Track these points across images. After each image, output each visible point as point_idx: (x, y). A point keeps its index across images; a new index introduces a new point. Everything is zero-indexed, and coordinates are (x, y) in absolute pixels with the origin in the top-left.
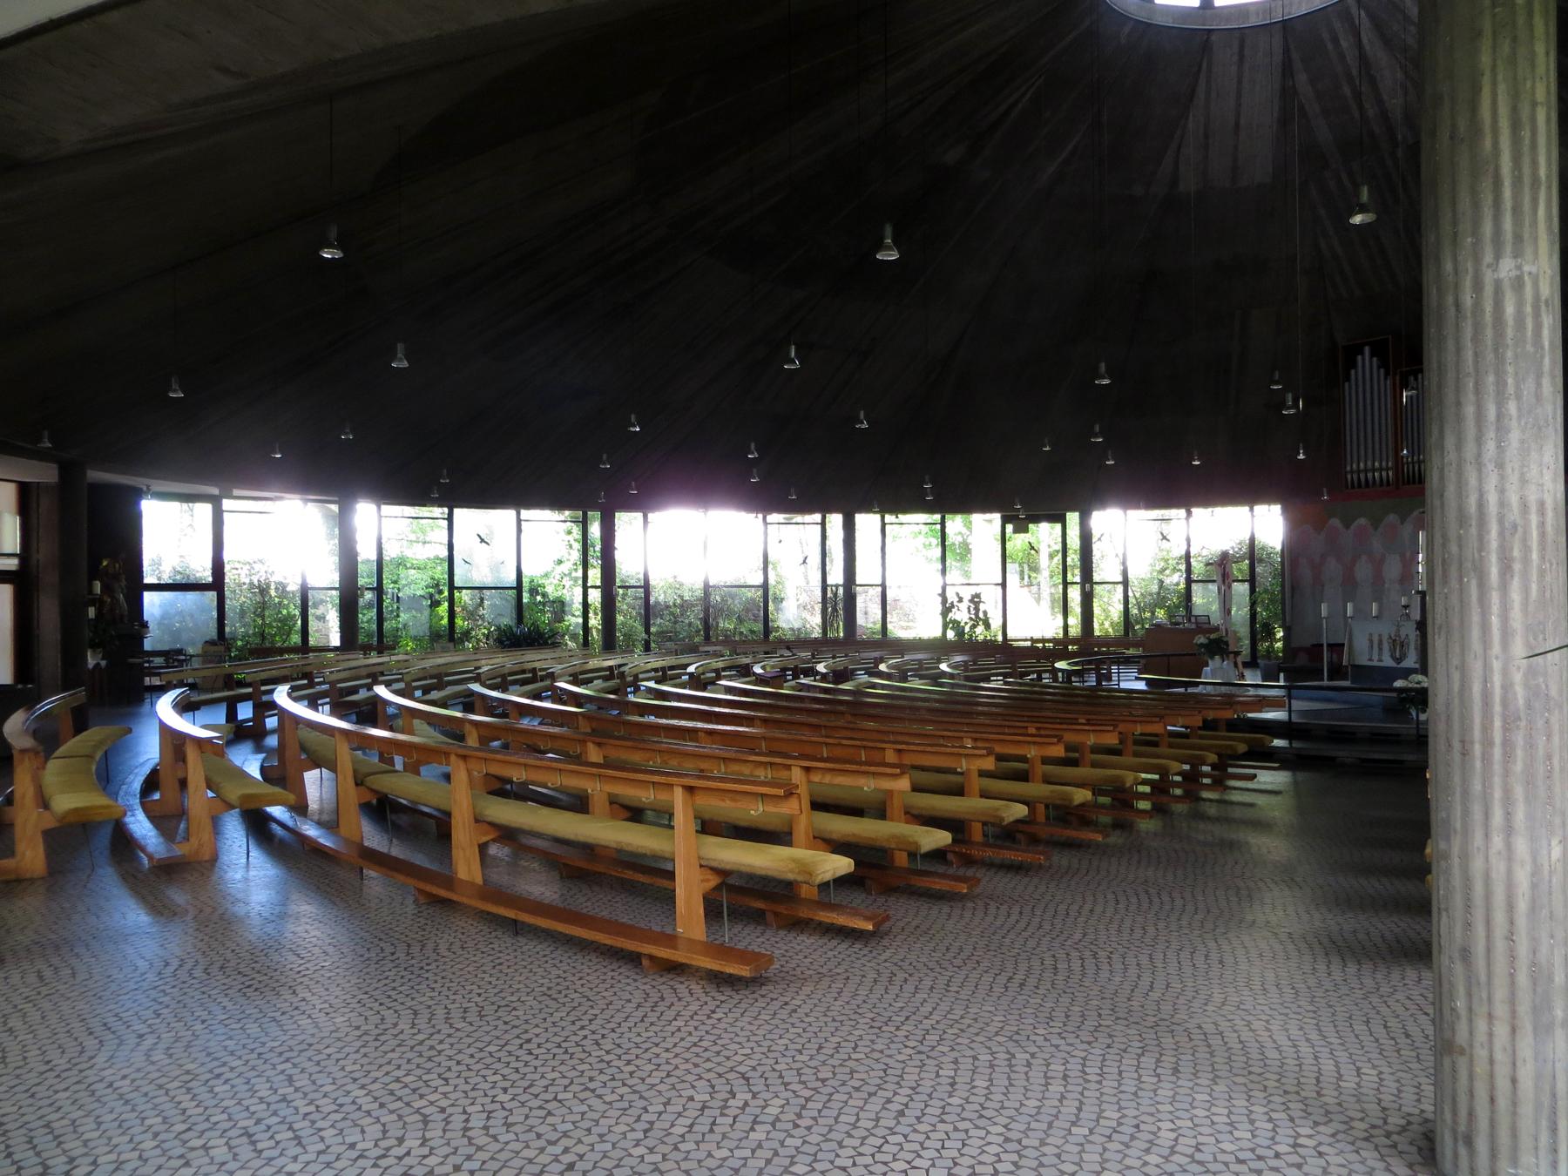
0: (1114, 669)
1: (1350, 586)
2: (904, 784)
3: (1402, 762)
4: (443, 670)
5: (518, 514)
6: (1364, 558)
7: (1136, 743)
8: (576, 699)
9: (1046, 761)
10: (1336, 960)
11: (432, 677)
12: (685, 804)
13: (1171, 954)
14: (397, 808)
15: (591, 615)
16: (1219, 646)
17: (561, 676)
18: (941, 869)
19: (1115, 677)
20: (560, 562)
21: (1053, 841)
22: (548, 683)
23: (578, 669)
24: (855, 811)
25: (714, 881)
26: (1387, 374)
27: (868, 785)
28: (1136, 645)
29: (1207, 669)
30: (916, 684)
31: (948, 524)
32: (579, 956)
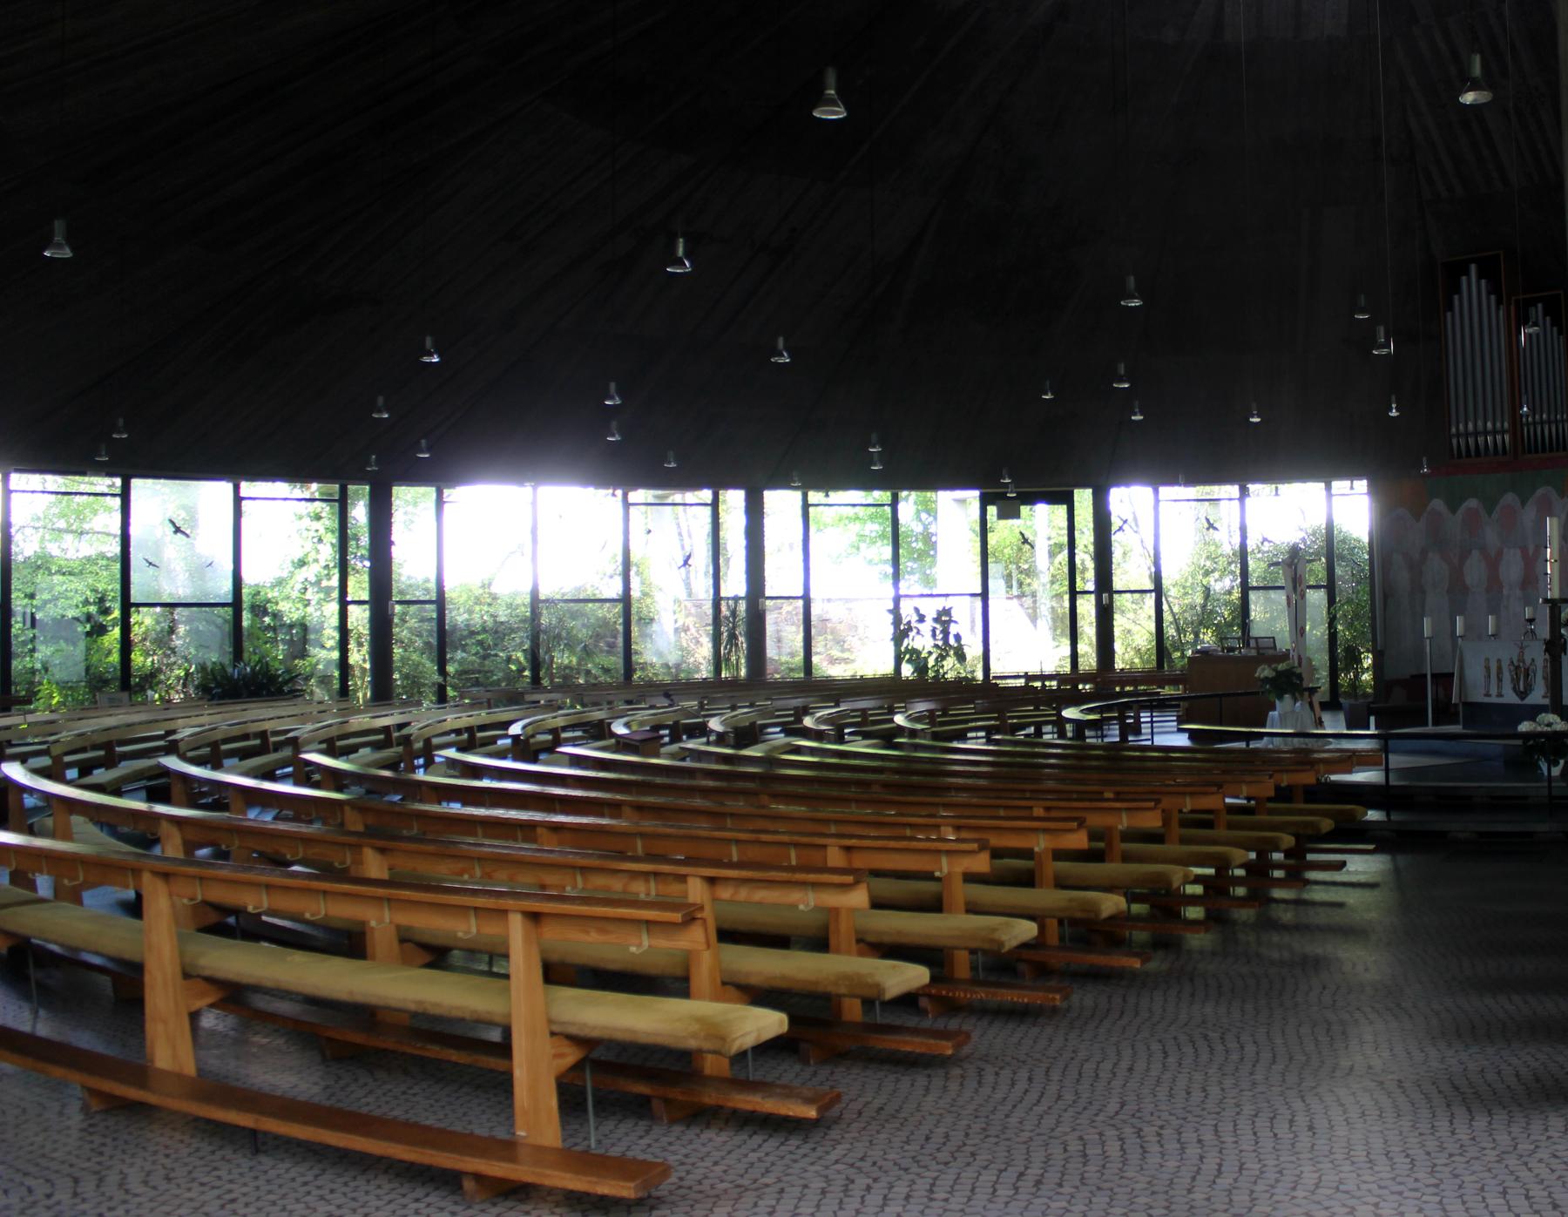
0: (1145, 717)
1: (1458, 594)
2: (858, 898)
3: (1530, 834)
4: (114, 736)
5: (237, 489)
6: (1476, 554)
7: (1184, 824)
8: (335, 779)
9: (1059, 855)
10: (1460, 1112)
11: (95, 747)
12: (527, 940)
13: (1244, 1126)
14: (46, 959)
15: (352, 645)
16: (1290, 682)
17: (309, 742)
18: (912, 1021)
19: (1146, 729)
20: (302, 563)
21: (1071, 971)
22: (287, 752)
23: (334, 732)
24: (777, 940)
25: (572, 1056)
26: (1499, 302)
27: (805, 903)
28: (1174, 681)
29: (1274, 714)
30: (859, 746)
31: (901, 506)
32: (361, 1181)
